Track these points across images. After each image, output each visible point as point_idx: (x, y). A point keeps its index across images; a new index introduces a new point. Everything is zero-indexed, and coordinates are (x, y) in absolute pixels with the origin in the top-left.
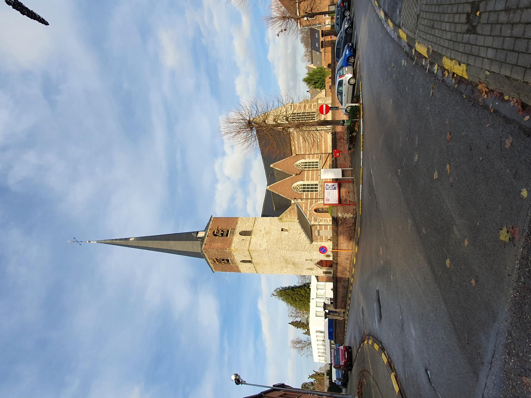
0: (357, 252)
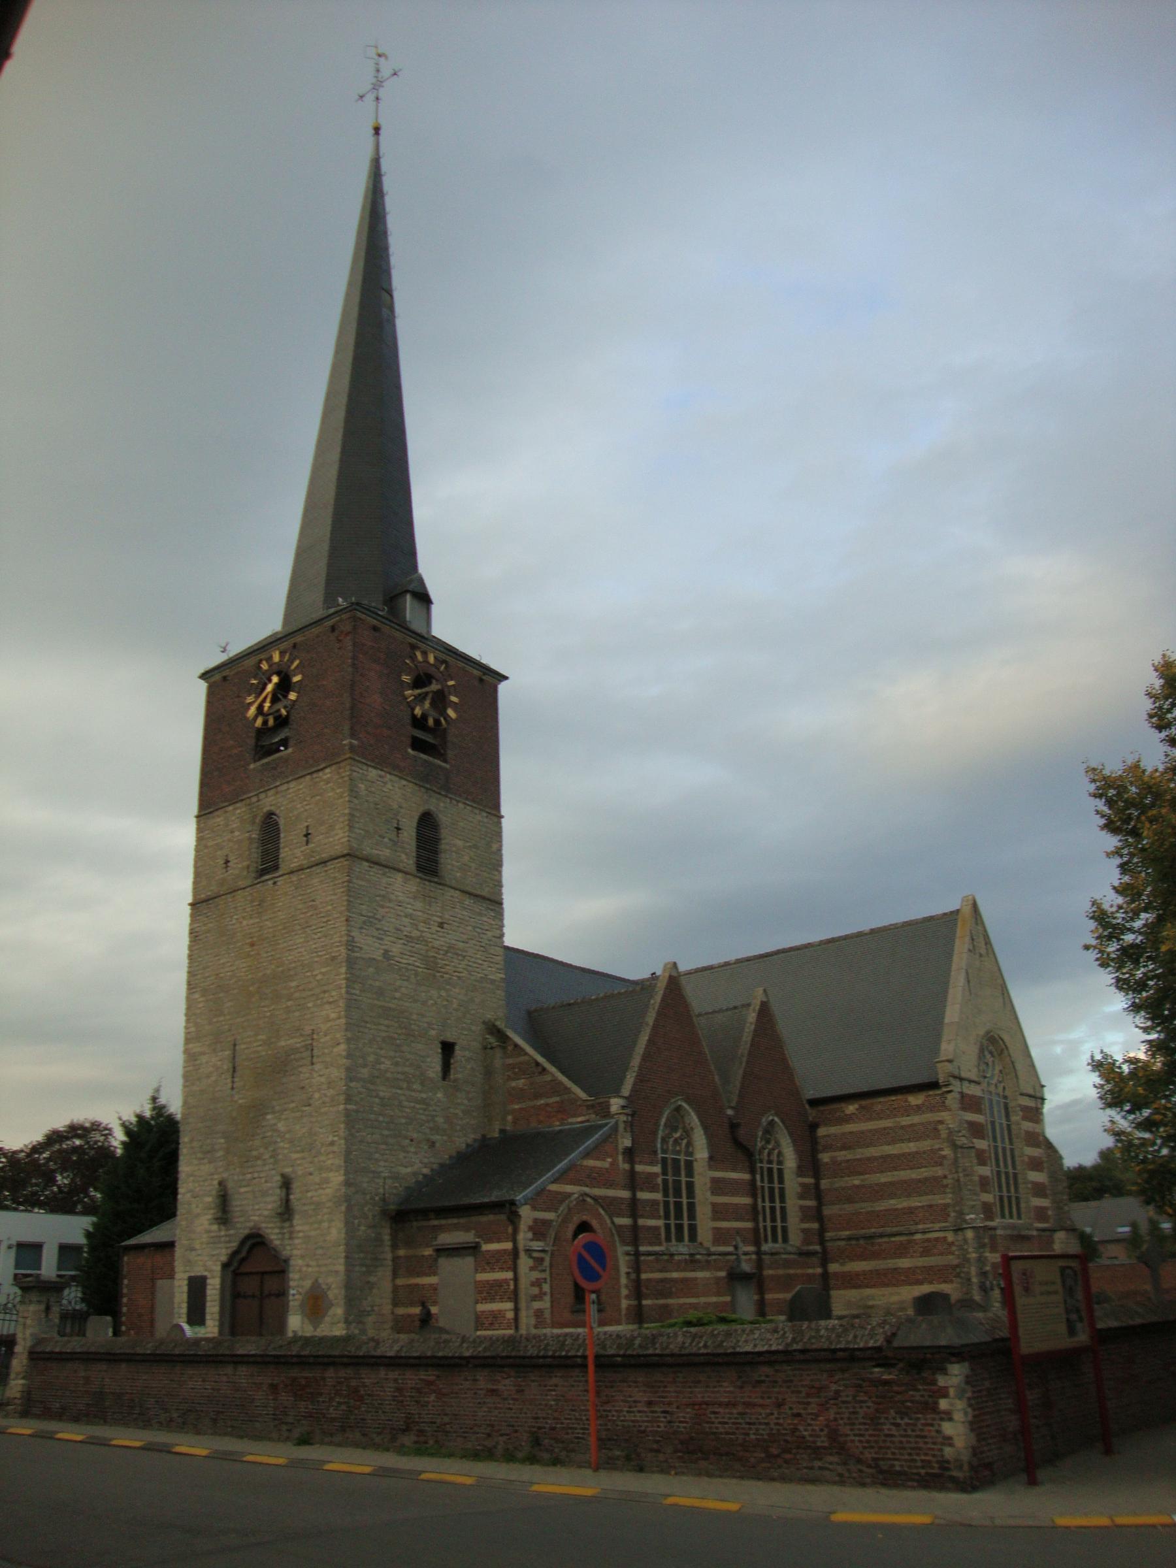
0: (59, 1439)
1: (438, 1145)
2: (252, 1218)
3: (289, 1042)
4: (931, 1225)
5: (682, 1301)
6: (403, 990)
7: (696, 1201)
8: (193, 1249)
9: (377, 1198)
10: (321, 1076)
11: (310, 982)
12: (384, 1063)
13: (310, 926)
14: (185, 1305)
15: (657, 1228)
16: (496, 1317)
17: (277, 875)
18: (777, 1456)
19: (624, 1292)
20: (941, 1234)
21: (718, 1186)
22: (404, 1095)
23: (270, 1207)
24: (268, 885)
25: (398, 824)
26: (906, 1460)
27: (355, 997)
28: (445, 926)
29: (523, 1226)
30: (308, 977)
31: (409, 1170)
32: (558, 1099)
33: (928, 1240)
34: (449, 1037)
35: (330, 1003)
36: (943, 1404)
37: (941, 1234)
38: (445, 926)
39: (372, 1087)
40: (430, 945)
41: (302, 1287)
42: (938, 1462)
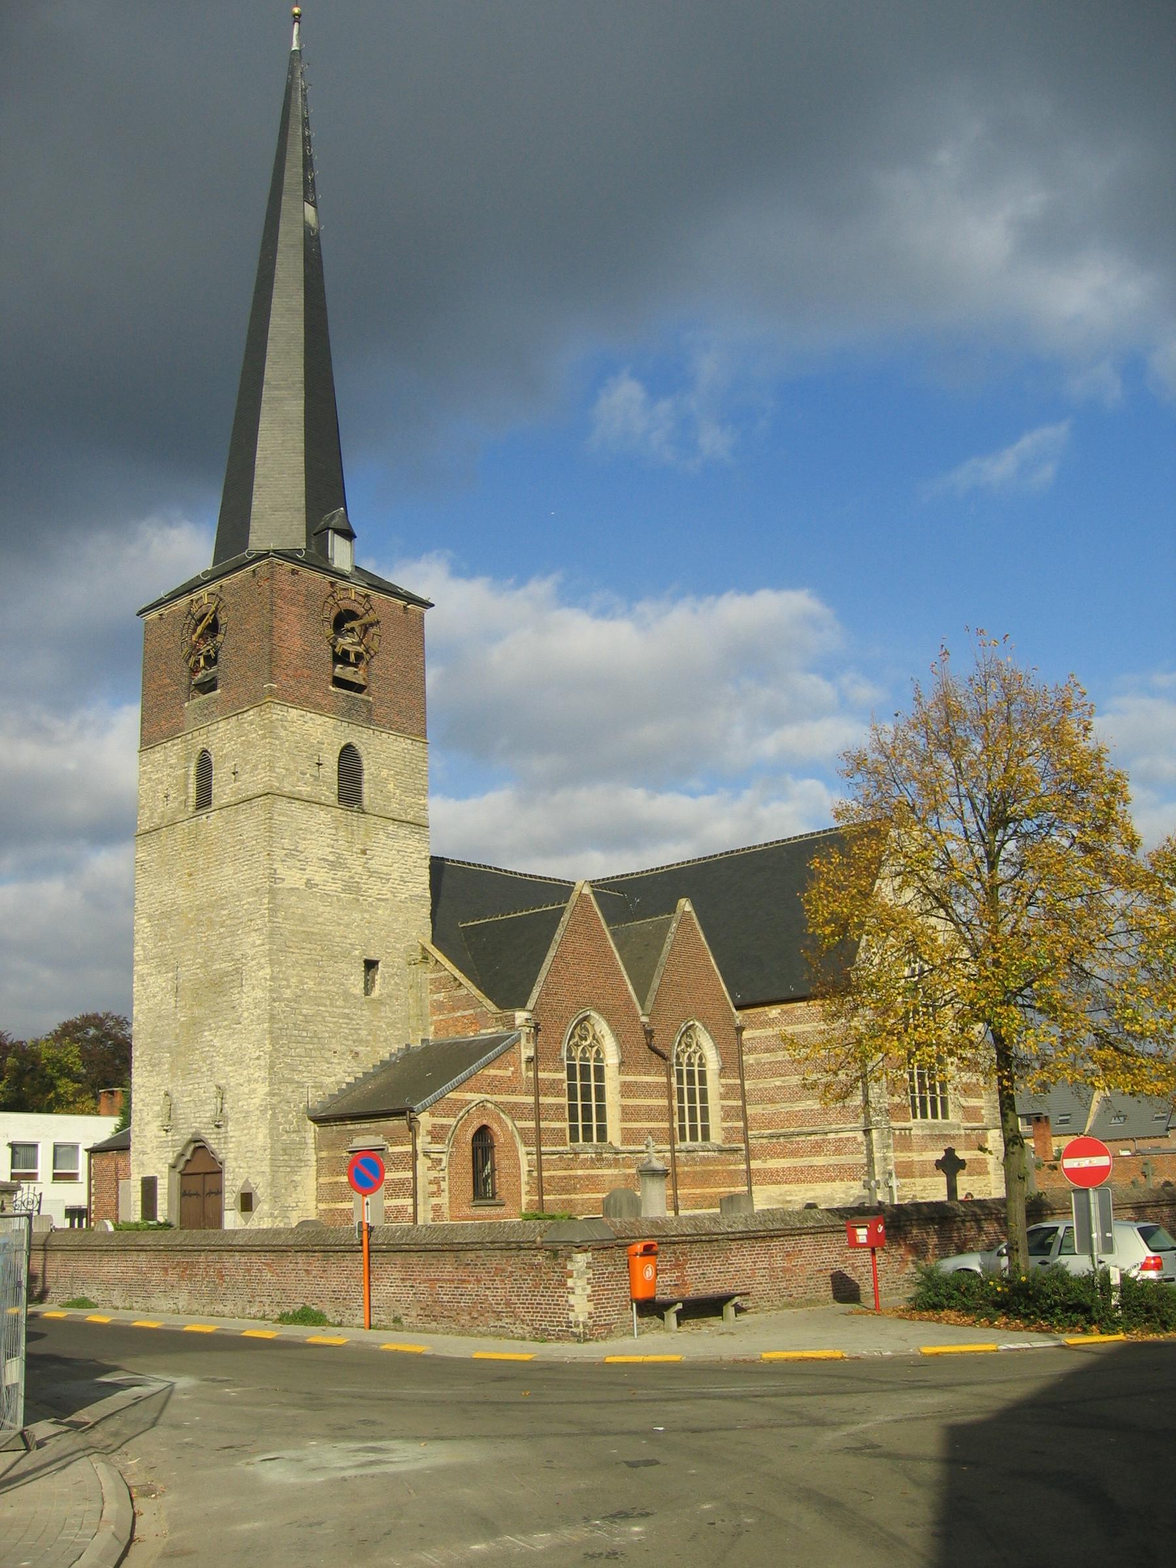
1: (361, 1055)
2: (193, 1125)
3: (222, 966)
4: (843, 1126)
5: (586, 1196)
6: (326, 915)
7: (607, 1103)
8: (144, 1153)
9: (301, 1106)
10: (248, 997)
11: (239, 911)
12: (307, 983)
13: (238, 859)
14: (139, 1203)
15: (562, 1130)
16: (400, 1210)
17: (209, 810)
18: (476, 1318)
19: (524, 1188)
20: (851, 1134)
21: (627, 1090)
22: (328, 1011)
23: (208, 1115)
24: (202, 819)
25: (319, 760)
26: (548, 1321)
27: (278, 925)
28: (368, 852)
29: (422, 1131)
30: (238, 906)
31: (333, 1079)
32: (471, 1012)
33: (841, 1140)
34: (373, 956)
35: (256, 931)
36: (570, 1283)
37: (851, 1134)
38: (368, 852)
39: (295, 1006)
40: (353, 871)
41: (235, 1186)
42: (565, 1322)
